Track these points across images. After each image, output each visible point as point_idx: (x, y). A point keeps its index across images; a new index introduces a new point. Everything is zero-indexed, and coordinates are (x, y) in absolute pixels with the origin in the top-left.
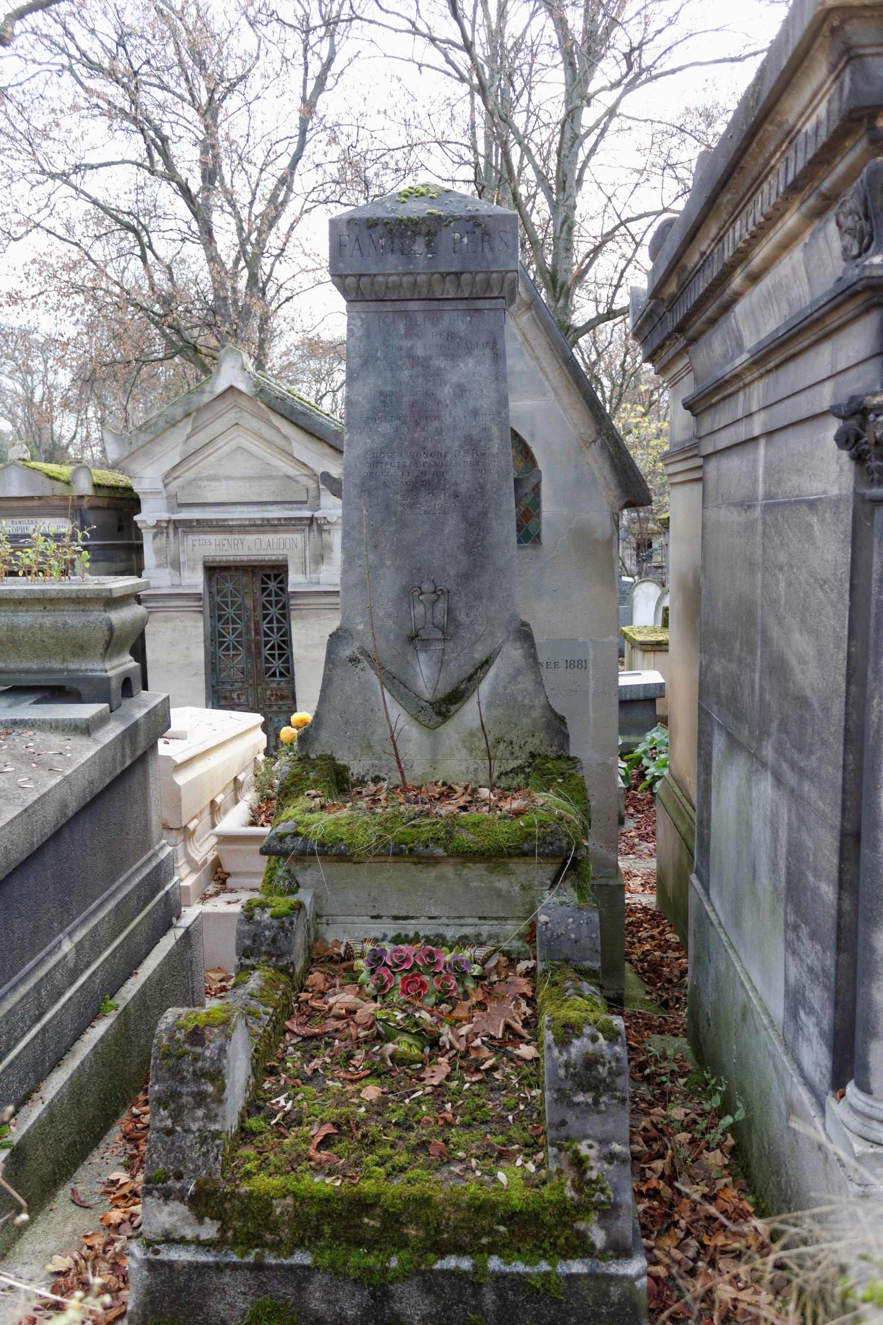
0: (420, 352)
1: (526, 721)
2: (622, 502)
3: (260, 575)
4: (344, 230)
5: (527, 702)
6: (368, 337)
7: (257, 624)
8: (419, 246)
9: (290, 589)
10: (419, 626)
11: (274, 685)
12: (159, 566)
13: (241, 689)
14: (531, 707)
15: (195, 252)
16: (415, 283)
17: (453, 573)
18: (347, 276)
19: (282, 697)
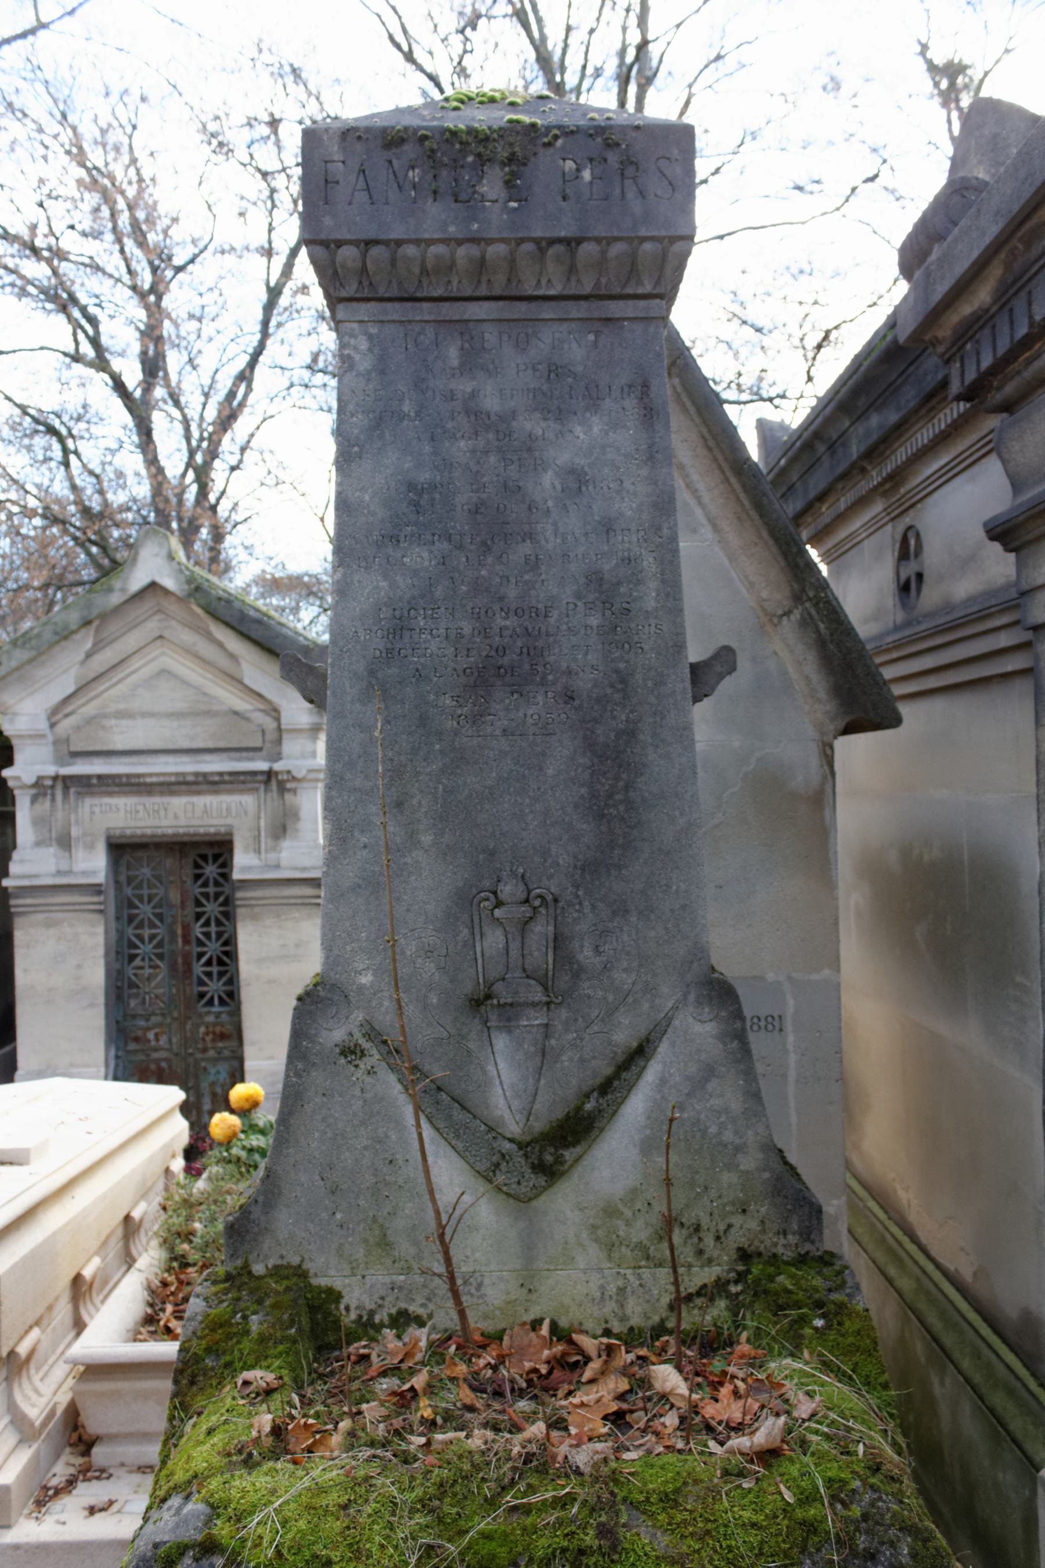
0: (491, 403)
1: (728, 1178)
2: (841, 724)
3: (192, 855)
4: (335, 151)
5: (728, 1136)
6: (382, 372)
7: (186, 928)
8: (491, 186)
9: (236, 875)
10: (493, 974)
11: (211, 1019)
12: (38, 844)
13: (160, 1025)
14: (739, 1149)
15: (132, 461)
16: (483, 258)
17: (564, 860)
18: (340, 244)
19: (223, 1037)
